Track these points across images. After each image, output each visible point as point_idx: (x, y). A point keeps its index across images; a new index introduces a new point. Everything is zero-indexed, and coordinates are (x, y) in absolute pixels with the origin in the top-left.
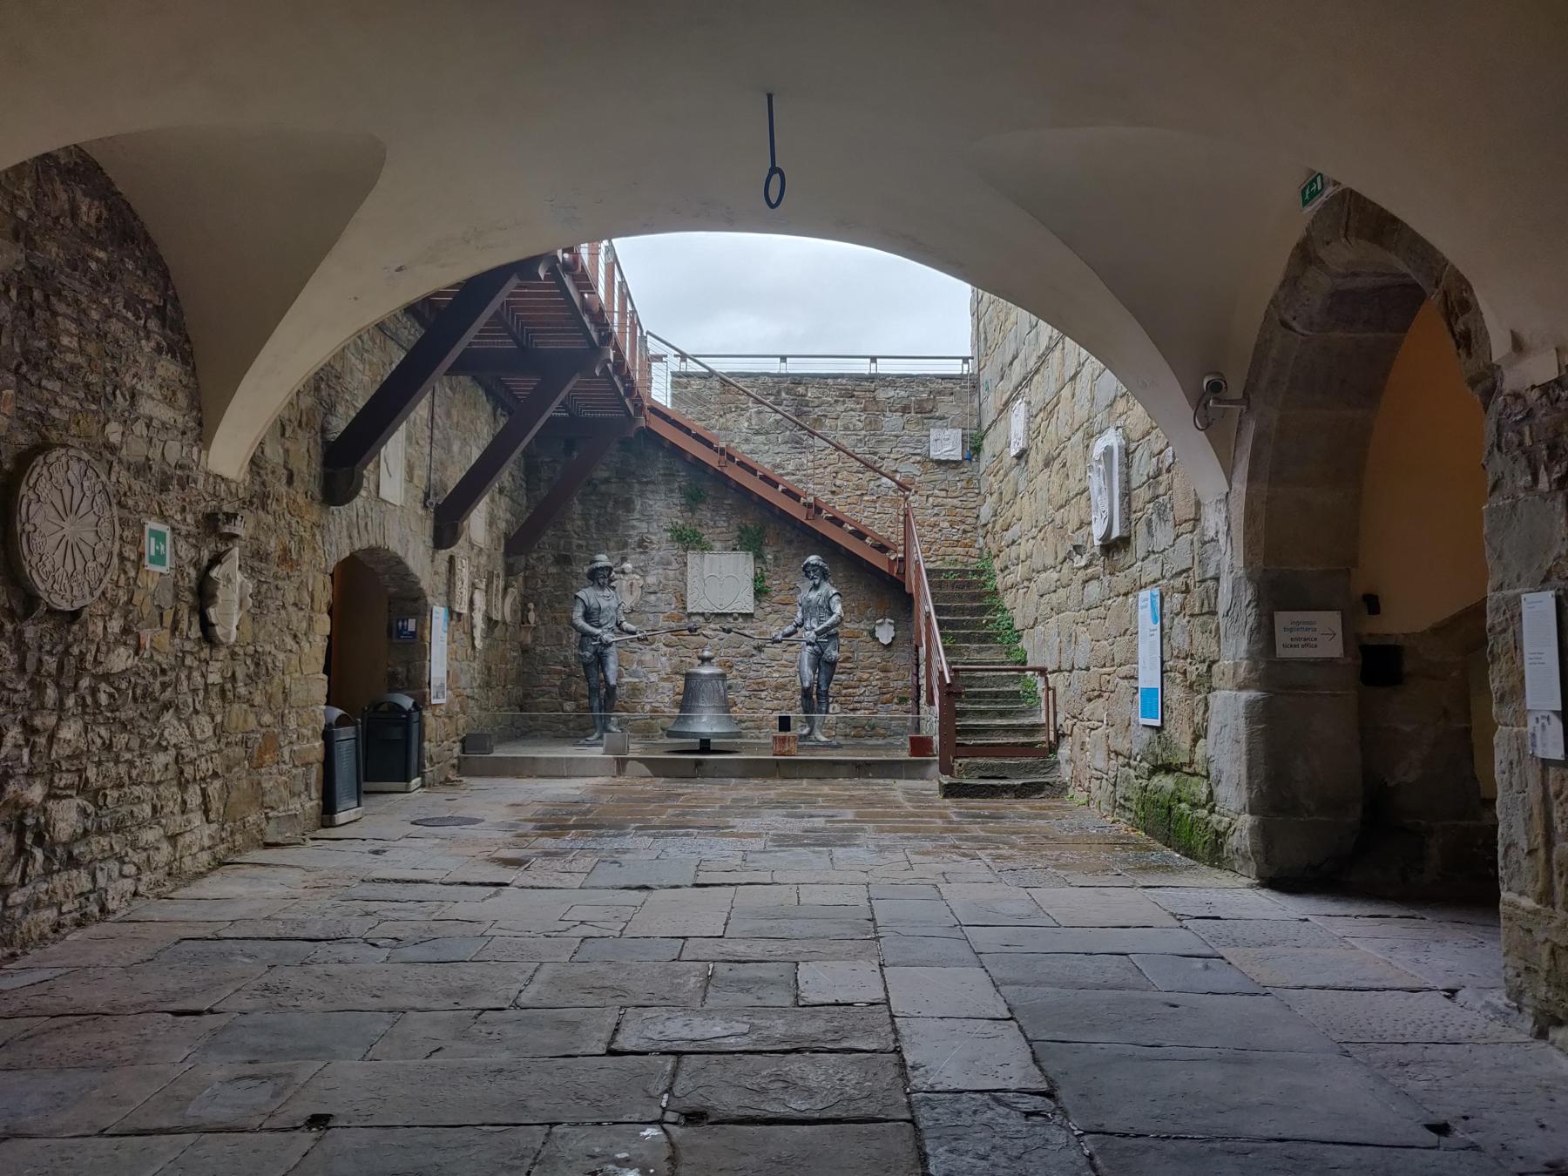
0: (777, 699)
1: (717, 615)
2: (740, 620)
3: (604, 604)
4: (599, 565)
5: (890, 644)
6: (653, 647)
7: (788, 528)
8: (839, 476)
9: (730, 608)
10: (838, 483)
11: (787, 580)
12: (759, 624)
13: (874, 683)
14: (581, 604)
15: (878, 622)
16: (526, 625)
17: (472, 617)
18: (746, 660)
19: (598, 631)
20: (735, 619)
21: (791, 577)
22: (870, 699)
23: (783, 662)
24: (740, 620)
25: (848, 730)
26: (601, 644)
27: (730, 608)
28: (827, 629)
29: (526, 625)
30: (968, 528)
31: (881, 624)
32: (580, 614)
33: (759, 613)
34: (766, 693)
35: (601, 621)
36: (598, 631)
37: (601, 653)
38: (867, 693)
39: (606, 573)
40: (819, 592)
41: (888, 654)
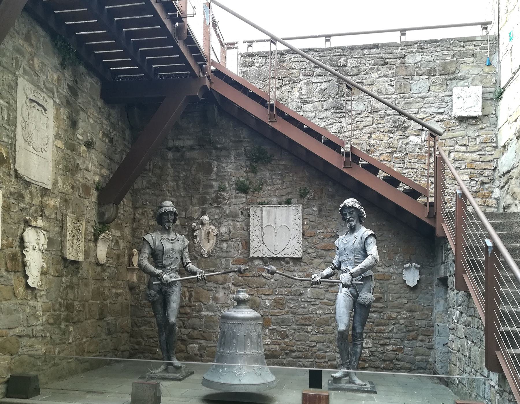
0: (320, 333)
1: (273, 259)
2: (291, 263)
3: (167, 246)
4: (164, 209)
5: (415, 287)
6: (225, 286)
7: (330, 183)
8: (373, 137)
9: (283, 253)
10: (372, 142)
11: (329, 229)
12: (306, 267)
13: (401, 322)
14: (147, 246)
15: (405, 266)
16: (131, 267)
17: (24, 256)
18: (295, 298)
19: (158, 271)
20: (287, 263)
21: (332, 226)
22: (398, 335)
23: (325, 301)
24: (291, 263)
25: (378, 363)
26: (162, 283)
27: (283, 253)
28: (363, 271)
29: (131, 267)
30: (486, 180)
31: (407, 269)
32: (146, 255)
33: (306, 258)
34: (311, 327)
35: (164, 262)
36: (158, 271)
37: (166, 292)
38: (395, 331)
39: (171, 218)
40: (355, 234)
41: (413, 296)
